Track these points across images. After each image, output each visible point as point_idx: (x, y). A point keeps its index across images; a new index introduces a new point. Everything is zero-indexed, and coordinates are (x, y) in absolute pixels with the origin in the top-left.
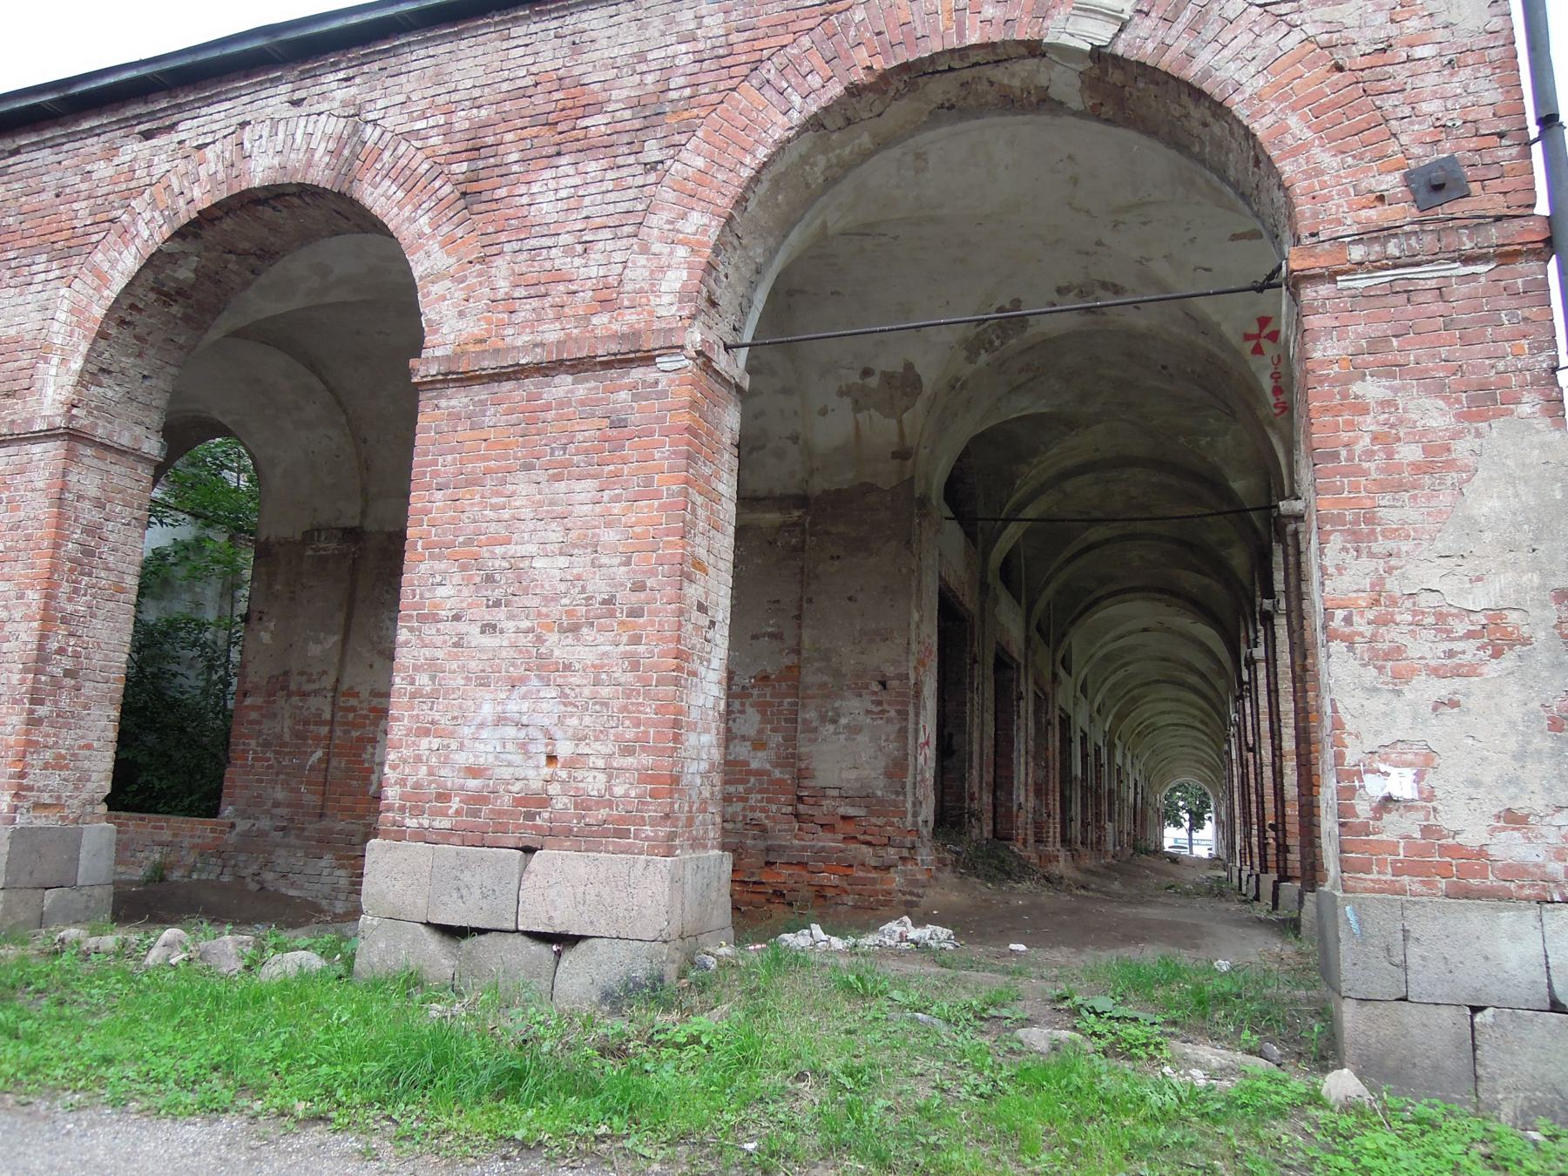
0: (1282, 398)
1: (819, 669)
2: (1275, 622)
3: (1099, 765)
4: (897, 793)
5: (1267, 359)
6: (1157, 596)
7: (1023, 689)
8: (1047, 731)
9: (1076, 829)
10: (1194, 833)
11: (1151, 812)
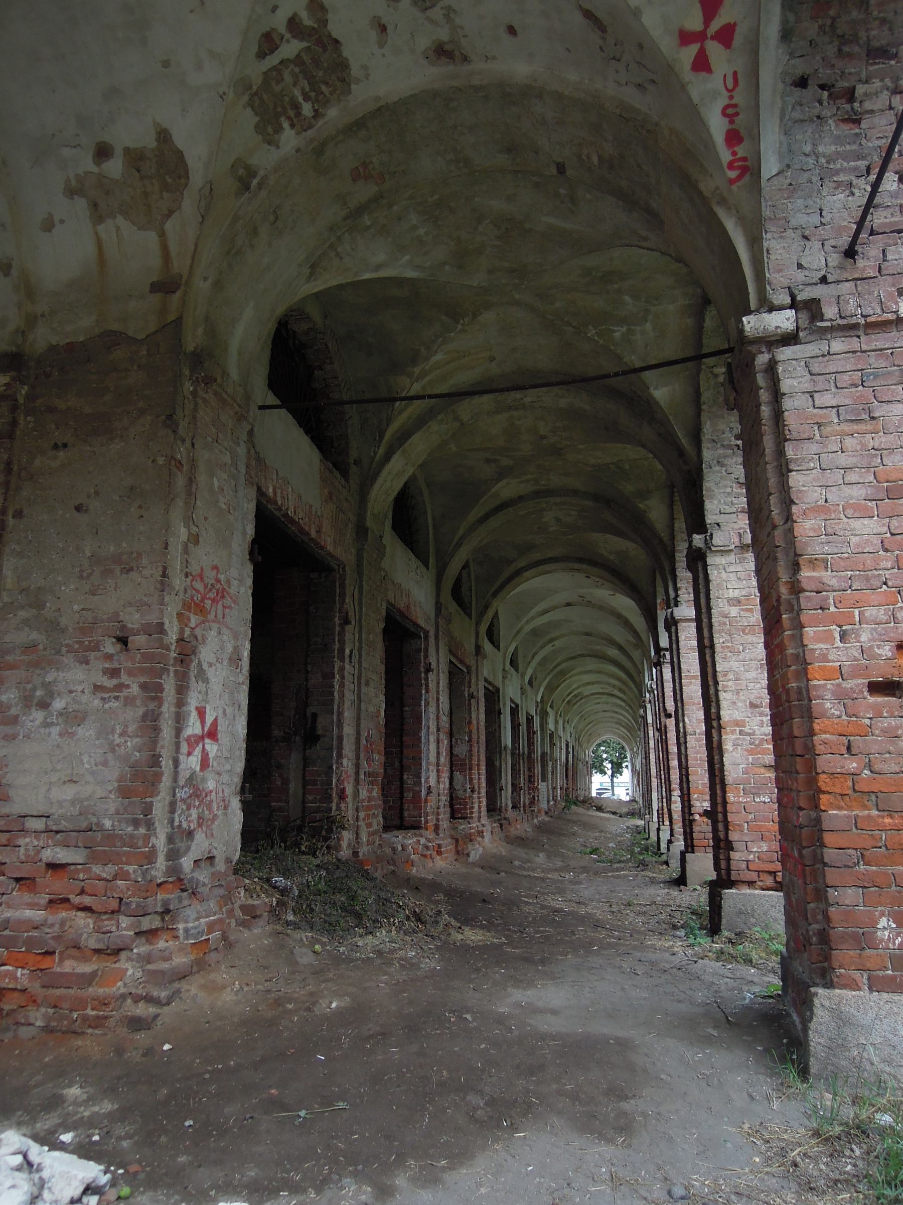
0: (741, 151)
1: (26, 622)
2: (710, 560)
3: (531, 732)
4: (136, 823)
5: (716, 81)
6: (577, 566)
7: (432, 660)
8: (470, 704)
9: (506, 798)
10: (615, 780)
11: (580, 766)
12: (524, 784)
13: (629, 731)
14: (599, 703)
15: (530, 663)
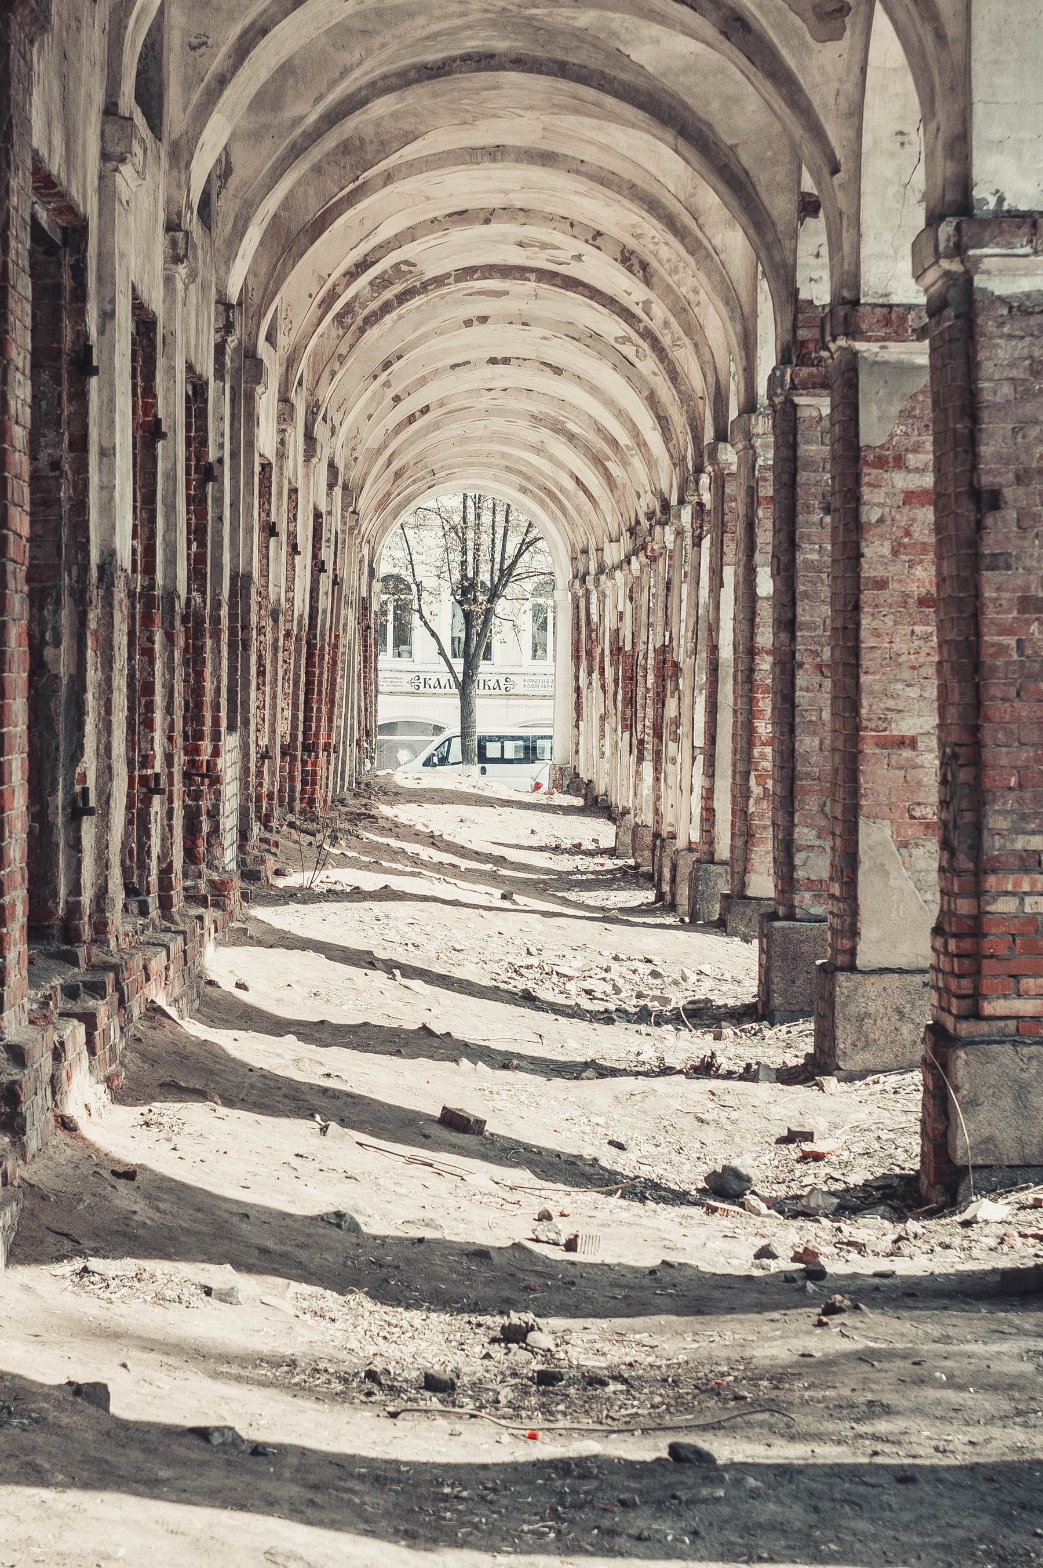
12: (169, 759)
13: (598, 461)
14: (483, 319)
15: (222, 81)
